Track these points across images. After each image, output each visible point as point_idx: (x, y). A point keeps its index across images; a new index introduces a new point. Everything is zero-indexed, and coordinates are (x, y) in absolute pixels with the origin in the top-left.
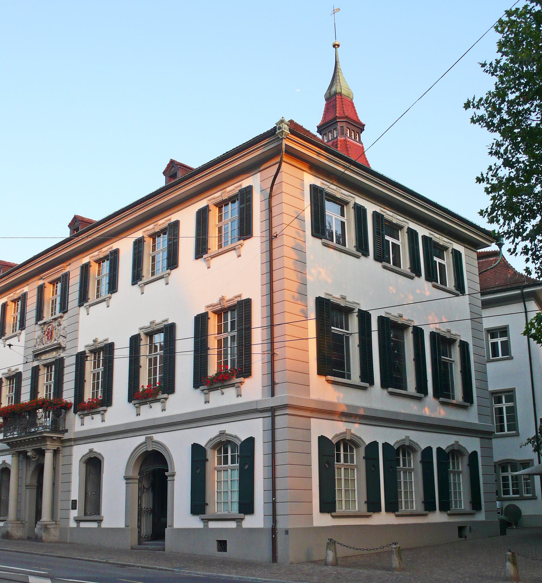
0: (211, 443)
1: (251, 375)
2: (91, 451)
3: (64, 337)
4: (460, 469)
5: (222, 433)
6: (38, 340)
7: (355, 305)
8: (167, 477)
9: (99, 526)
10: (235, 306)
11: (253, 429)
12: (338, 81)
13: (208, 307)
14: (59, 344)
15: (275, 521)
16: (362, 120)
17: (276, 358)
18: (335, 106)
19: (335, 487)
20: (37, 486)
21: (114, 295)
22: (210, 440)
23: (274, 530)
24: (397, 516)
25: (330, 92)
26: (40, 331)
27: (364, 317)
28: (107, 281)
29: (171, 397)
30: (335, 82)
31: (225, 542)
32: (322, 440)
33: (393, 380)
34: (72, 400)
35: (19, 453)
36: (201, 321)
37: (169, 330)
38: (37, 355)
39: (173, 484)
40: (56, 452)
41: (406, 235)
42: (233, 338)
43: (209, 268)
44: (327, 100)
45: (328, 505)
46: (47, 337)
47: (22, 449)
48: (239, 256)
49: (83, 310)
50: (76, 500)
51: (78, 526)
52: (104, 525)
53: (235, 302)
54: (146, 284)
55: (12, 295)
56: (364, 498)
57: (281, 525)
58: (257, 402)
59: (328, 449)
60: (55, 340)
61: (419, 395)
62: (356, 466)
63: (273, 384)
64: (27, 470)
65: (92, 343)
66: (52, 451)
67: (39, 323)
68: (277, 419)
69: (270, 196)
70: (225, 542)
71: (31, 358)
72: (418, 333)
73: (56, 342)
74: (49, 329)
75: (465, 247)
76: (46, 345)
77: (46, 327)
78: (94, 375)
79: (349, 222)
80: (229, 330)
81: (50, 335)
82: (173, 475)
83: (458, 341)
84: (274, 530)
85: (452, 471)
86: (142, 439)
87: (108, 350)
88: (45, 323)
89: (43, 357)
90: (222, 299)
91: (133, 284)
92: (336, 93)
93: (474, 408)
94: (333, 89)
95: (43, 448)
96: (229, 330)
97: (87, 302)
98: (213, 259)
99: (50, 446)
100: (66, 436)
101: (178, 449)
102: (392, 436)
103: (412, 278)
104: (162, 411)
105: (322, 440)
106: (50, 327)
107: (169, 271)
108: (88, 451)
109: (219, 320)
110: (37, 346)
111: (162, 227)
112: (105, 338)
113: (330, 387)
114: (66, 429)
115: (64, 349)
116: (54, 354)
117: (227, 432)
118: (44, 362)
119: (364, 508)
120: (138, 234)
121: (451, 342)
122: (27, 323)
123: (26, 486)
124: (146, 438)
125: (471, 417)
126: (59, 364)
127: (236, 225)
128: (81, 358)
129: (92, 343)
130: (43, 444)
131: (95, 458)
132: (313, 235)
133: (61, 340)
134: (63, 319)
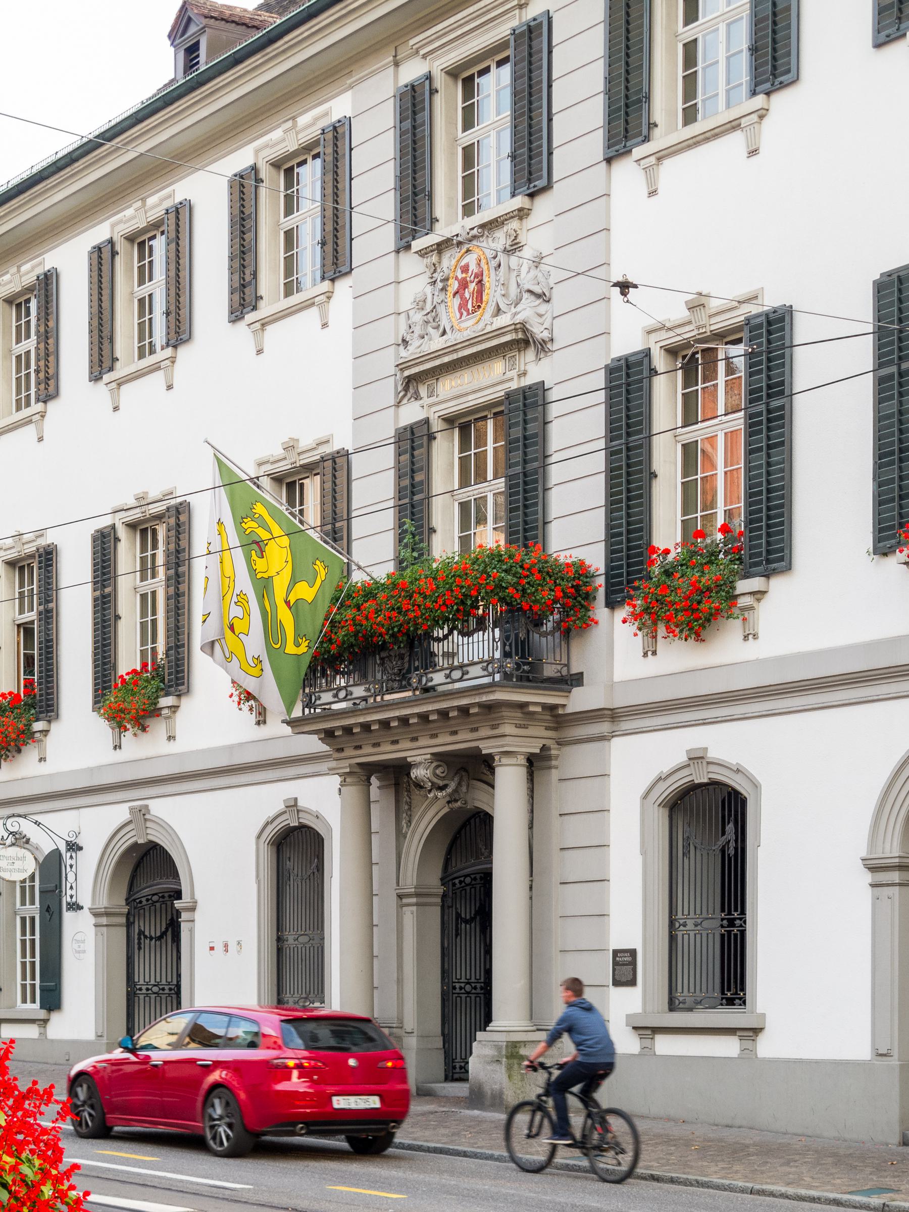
0: (662, 786)
1: (789, 568)
2: (293, 806)
3: (538, 296)
5: (697, 758)
6: (418, 317)
8: (178, 913)
9: (43, 1034)
10: (738, 329)
13: (649, 333)
14: (523, 327)
20: (444, 896)
21: (780, 100)
26: (425, 279)
28: (507, 148)
29: (777, 584)
34: (596, 559)
35: (368, 770)
36: (104, 545)
37: (769, 337)
38: (413, 382)
39: (191, 931)
40: (535, 764)
42: (730, 436)
46: (457, 301)
47: (387, 753)
49: (627, 172)
50: (633, 953)
51: (647, 1051)
52: (768, 1047)
53: (737, 317)
54: (661, 156)
55: (277, 134)
60: (498, 311)
64: (400, 835)
65: (279, 452)
66: (522, 760)
67: (417, 245)
71: (388, 390)
73: (504, 320)
74: (465, 269)
76: (452, 338)
77: (449, 260)
78: (144, 597)
80: (490, 476)
81: (472, 292)
88: (441, 247)
89: (448, 386)
91: (95, 377)
95: (487, 748)
96: (490, 476)
97: (647, 139)
99: (510, 744)
100: (579, 700)
107: (759, 101)
108: (683, 758)
109: (465, 444)
110: (415, 343)
111: (306, 137)
112: (321, 435)
114: (574, 671)
115: (543, 347)
116: (497, 368)
117: (712, 754)
118: (453, 407)
120: (241, 158)
122: (361, 250)
123: (400, 897)
124: (131, 809)
126: (524, 414)
127: (742, 38)
128: (627, 383)
129: (279, 452)
130: (485, 732)
131: (303, 829)
133: (527, 311)
134: (531, 222)
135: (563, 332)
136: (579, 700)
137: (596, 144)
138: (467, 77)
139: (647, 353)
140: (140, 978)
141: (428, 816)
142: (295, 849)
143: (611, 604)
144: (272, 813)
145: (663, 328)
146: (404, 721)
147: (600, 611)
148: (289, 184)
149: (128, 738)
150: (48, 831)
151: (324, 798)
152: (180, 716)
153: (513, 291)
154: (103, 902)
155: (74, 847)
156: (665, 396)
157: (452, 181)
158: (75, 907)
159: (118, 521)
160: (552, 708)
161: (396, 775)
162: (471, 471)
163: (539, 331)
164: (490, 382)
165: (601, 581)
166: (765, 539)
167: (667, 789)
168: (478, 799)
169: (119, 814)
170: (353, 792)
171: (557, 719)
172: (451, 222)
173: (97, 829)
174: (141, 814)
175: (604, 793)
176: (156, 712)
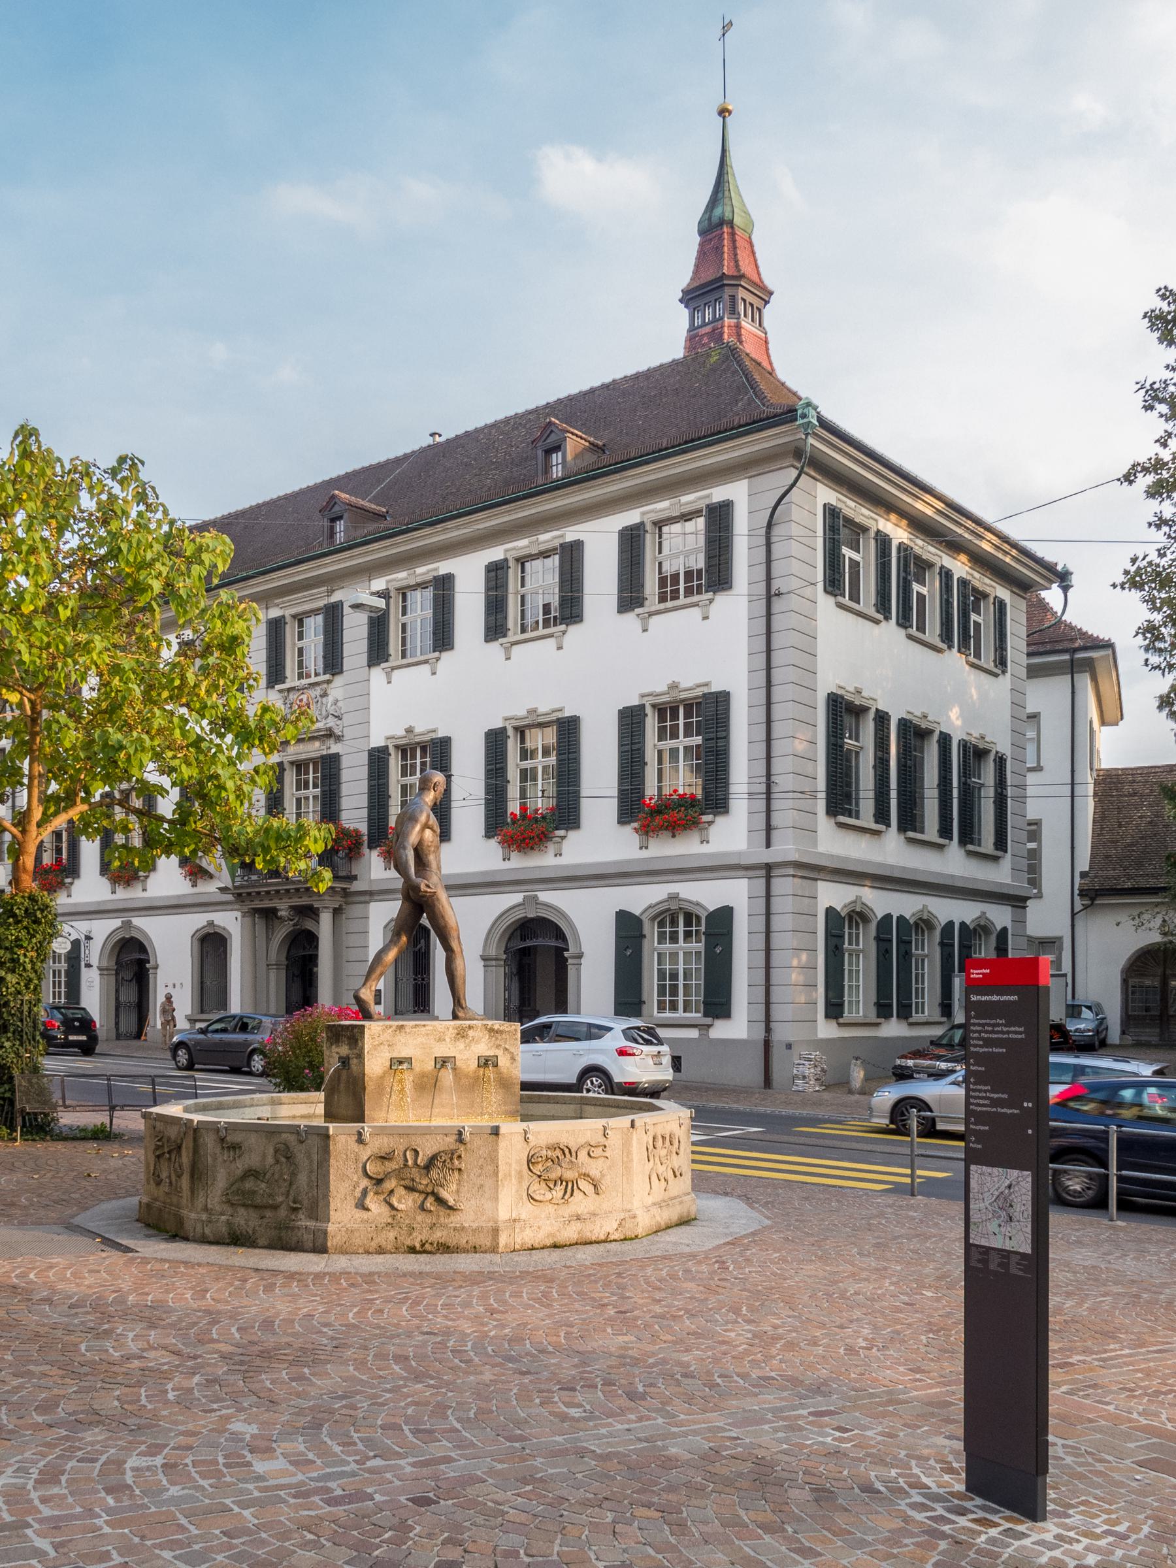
0: (651, 910)
4: (861, 946)
5: (211, 923)
7: (871, 702)
8: (148, 970)
11: (736, 894)
12: (726, 193)
13: (643, 696)
15: (768, 1030)
16: (769, 282)
17: (774, 789)
18: (719, 250)
19: (843, 980)
22: (650, 907)
23: (767, 1044)
24: (911, 1024)
25: (710, 218)
27: (882, 719)
30: (720, 195)
31: (680, 1057)
32: (830, 911)
33: (910, 821)
34: (363, 828)
39: (578, 971)
40: (337, 912)
41: (873, 542)
43: (645, 630)
44: (701, 233)
45: (834, 1010)
48: (705, 618)
49: (377, 674)
53: (699, 692)
54: (393, 668)
56: (873, 998)
57: (781, 1034)
58: (740, 854)
59: (838, 926)
61: (942, 841)
62: (862, 951)
63: (769, 828)
64: (268, 939)
65: (402, 733)
68: (774, 881)
69: (770, 526)
70: (680, 1057)
72: (945, 740)
74: (301, 700)
75: (1012, 592)
77: (293, 696)
79: (867, 564)
82: (580, 956)
83: (873, 711)
84: (767, 1044)
85: (848, 950)
86: (517, 898)
87: (438, 752)
90: (674, 686)
92: (722, 222)
93: (1007, 862)
94: (718, 212)
98: (514, 647)
100: (357, 886)
101: (590, 919)
102: (905, 905)
103: (877, 622)
104: (641, 848)
105: (830, 911)
106: (304, 697)
107: (437, 654)
108: (665, 896)
113: (842, 833)
115: (339, 739)
119: (873, 1012)
121: (858, 711)
125: (1001, 875)
126: (330, 767)
128: (378, 759)
132: (825, 591)
133: (331, 722)
134: (332, 685)
135: (348, 733)
136: (357, 886)
137: (364, 659)
138: (300, 619)
139: (505, 728)
140: (122, 999)
141: (281, 933)
142: (212, 945)
143: (370, 847)
144: (200, 926)
145: (393, 738)
146: (278, 892)
147: (366, 850)
148: (523, 571)
149: (652, 842)
150: (77, 930)
151: (230, 921)
152: (149, 881)
153: (324, 713)
154: (105, 964)
155: (88, 938)
156: (394, 764)
157: (293, 661)
158: (88, 966)
159: (647, 702)
160: (344, 889)
161: (269, 915)
162: (302, 785)
163: (337, 732)
164: (314, 749)
165: (366, 838)
166: (567, 814)
167: (198, 935)
168: (309, 925)
169: (116, 923)
170: (248, 920)
171: (346, 893)
172: (293, 680)
173: (102, 930)
174: (127, 925)
175: (367, 925)
176: (137, 878)
